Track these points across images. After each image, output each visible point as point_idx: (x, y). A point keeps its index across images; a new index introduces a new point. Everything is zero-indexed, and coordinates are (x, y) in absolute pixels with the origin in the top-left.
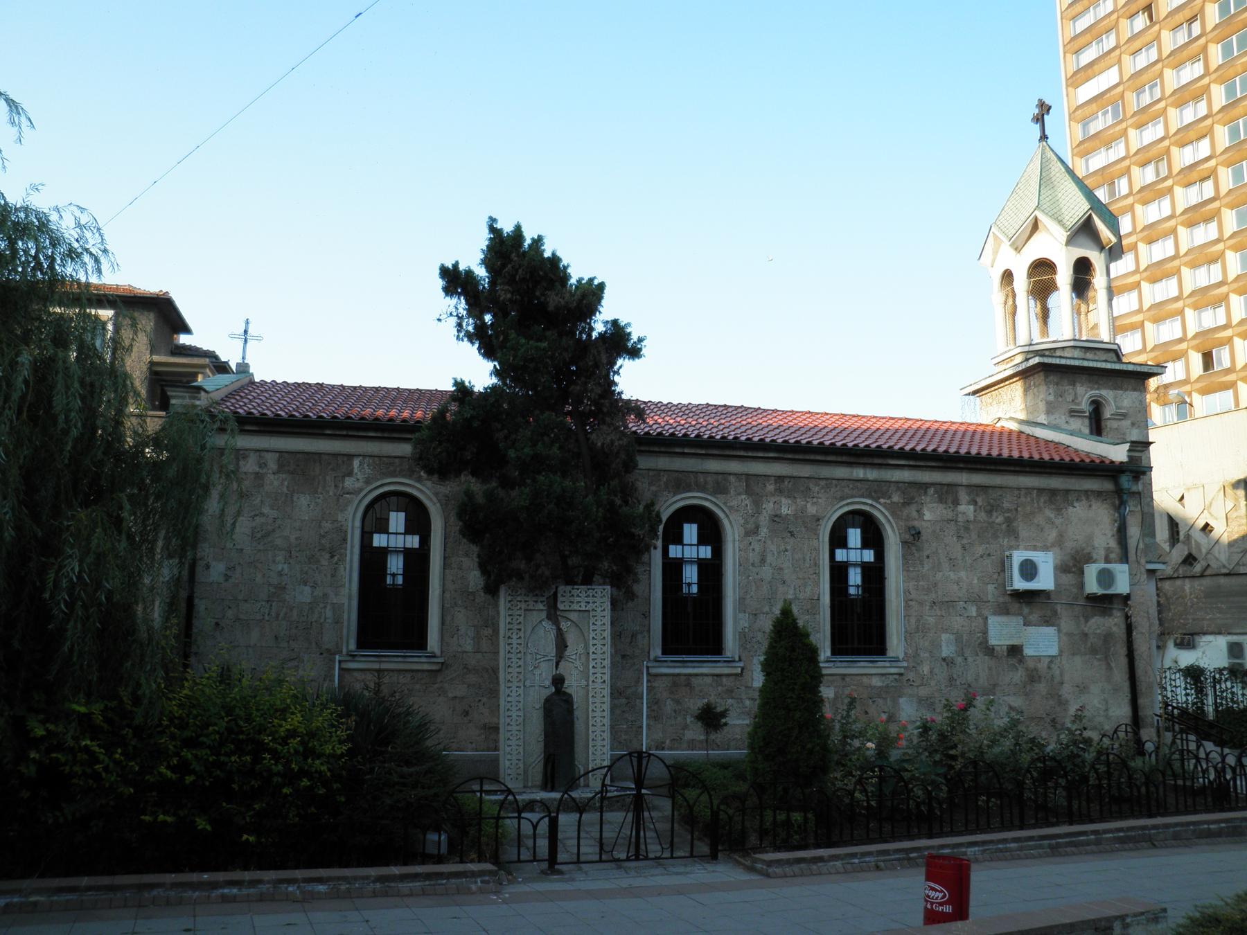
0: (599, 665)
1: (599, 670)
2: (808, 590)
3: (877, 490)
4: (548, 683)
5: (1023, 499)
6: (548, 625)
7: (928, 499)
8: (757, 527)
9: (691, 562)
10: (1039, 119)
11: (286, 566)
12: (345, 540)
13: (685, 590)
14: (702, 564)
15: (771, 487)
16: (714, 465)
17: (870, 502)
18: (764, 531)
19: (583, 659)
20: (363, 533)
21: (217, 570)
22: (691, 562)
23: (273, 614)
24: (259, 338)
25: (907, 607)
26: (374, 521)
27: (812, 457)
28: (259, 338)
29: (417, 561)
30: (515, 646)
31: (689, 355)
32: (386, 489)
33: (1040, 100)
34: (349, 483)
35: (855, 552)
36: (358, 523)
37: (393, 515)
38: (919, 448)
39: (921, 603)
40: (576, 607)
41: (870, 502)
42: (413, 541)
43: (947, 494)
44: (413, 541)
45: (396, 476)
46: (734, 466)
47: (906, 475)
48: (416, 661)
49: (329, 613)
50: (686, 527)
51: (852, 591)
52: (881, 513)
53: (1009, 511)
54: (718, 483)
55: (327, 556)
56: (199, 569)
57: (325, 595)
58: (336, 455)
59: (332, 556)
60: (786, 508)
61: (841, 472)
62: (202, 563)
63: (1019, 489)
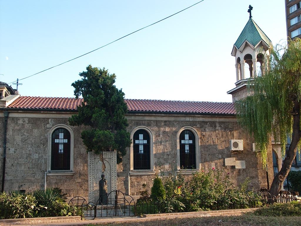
0: (114, 172)
1: (114, 173)
2: (173, 152)
3: (193, 124)
4: (100, 177)
5: (235, 125)
6: (100, 162)
7: (207, 126)
8: (159, 135)
9: (141, 144)
10: (249, 11)
11: (31, 149)
12: (47, 141)
13: (140, 152)
14: (144, 145)
15: (163, 124)
16: (147, 118)
17: (191, 127)
18: (161, 136)
19: (110, 170)
20: (52, 139)
21: (12, 151)
22: (141, 144)
23: (28, 162)
24: (21, 84)
25: (201, 155)
26: (55, 136)
27: (174, 115)
28: (21, 84)
29: (67, 146)
30: (92, 168)
31: (135, 86)
32: (58, 127)
33: (250, 5)
34: (48, 126)
35: (187, 141)
36: (51, 136)
37: (60, 134)
38: (64, 107)
39: (205, 155)
40: (107, 157)
41: (191, 127)
42: (66, 141)
43: (213, 125)
44: (66, 141)
45: (61, 124)
46: (153, 118)
47: (201, 119)
48: (67, 173)
49: (43, 161)
50: (140, 135)
51: (186, 151)
52: (194, 130)
53: (231, 128)
54: (148, 123)
55: (42, 146)
56: (7, 150)
57: (42, 156)
58: (44, 118)
59: (44, 146)
60: (167, 129)
61: (182, 119)
62: (8, 148)
63: (234, 122)
